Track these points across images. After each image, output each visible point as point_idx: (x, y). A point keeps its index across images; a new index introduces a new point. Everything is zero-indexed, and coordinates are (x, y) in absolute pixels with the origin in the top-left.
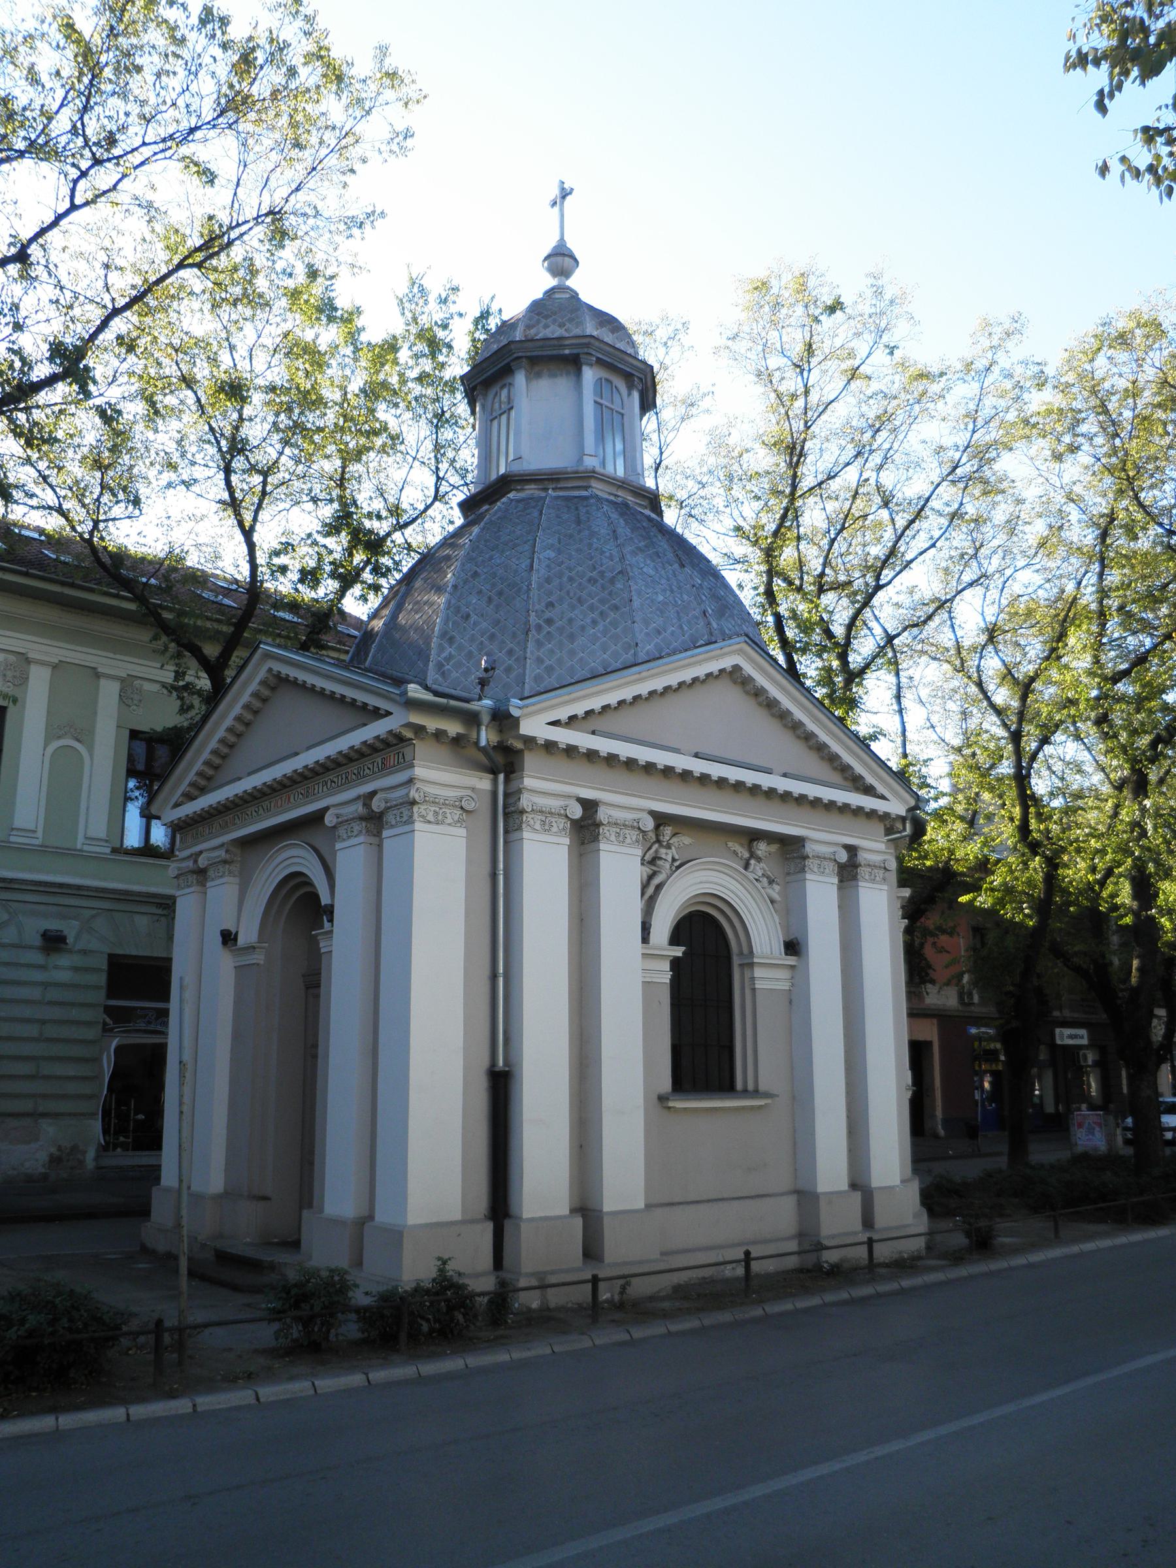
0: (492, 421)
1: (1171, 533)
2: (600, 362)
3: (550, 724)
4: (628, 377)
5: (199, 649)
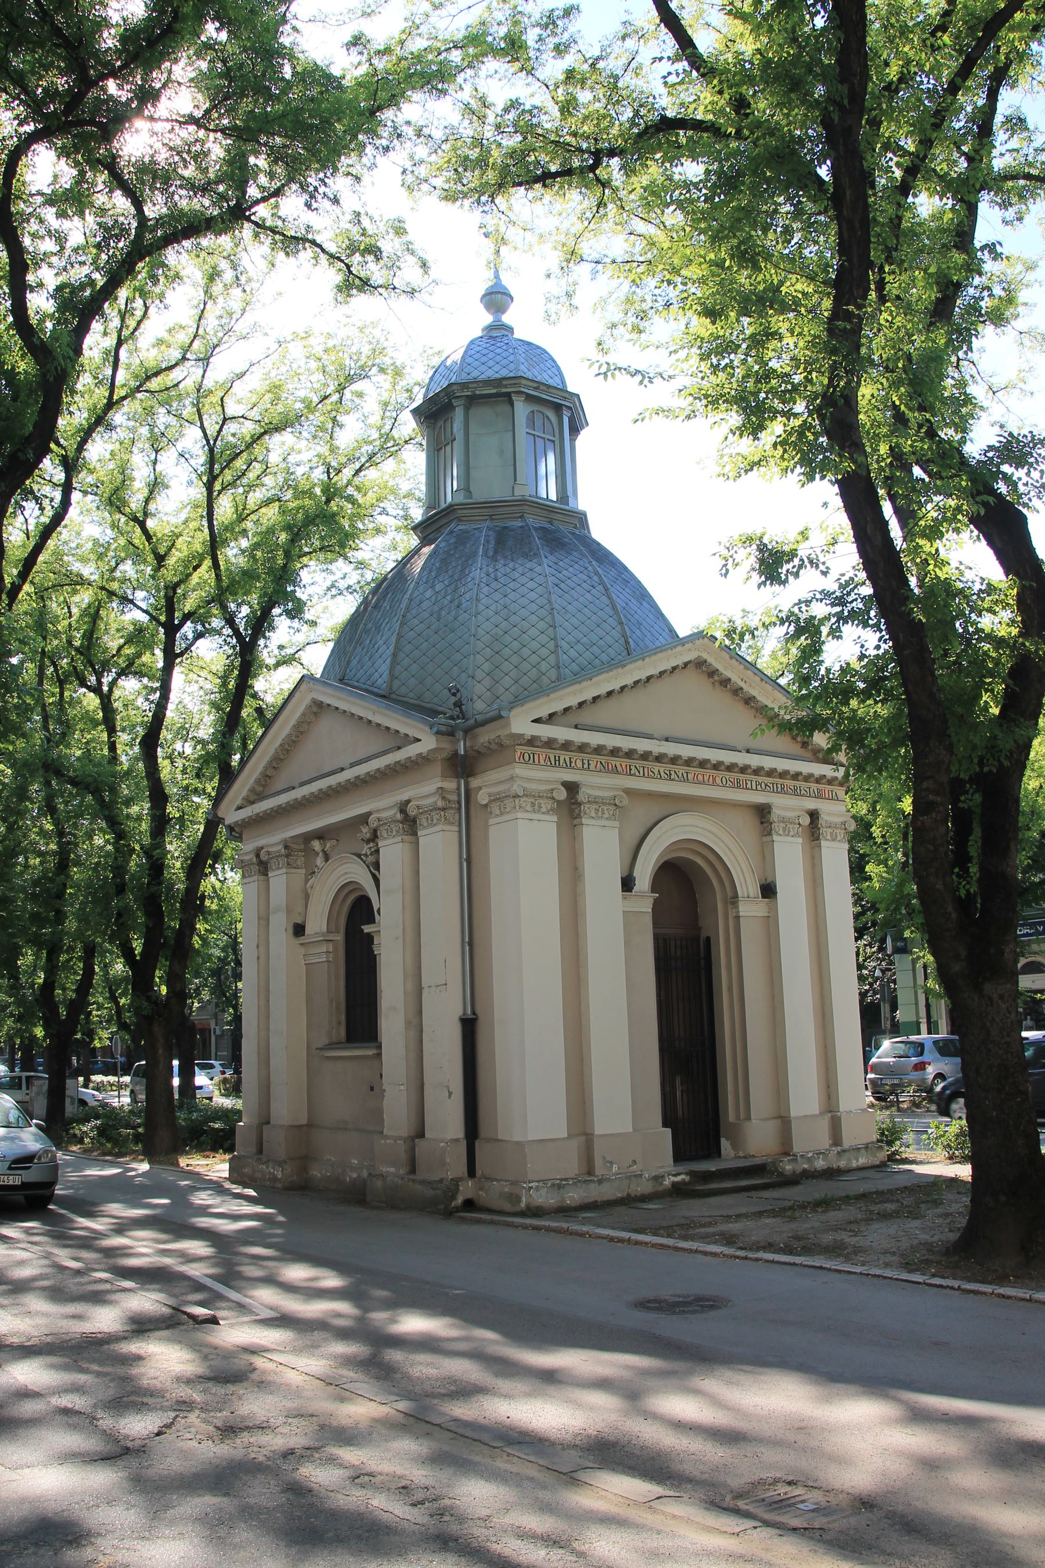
2: (530, 398)
3: (534, 721)
4: (558, 408)
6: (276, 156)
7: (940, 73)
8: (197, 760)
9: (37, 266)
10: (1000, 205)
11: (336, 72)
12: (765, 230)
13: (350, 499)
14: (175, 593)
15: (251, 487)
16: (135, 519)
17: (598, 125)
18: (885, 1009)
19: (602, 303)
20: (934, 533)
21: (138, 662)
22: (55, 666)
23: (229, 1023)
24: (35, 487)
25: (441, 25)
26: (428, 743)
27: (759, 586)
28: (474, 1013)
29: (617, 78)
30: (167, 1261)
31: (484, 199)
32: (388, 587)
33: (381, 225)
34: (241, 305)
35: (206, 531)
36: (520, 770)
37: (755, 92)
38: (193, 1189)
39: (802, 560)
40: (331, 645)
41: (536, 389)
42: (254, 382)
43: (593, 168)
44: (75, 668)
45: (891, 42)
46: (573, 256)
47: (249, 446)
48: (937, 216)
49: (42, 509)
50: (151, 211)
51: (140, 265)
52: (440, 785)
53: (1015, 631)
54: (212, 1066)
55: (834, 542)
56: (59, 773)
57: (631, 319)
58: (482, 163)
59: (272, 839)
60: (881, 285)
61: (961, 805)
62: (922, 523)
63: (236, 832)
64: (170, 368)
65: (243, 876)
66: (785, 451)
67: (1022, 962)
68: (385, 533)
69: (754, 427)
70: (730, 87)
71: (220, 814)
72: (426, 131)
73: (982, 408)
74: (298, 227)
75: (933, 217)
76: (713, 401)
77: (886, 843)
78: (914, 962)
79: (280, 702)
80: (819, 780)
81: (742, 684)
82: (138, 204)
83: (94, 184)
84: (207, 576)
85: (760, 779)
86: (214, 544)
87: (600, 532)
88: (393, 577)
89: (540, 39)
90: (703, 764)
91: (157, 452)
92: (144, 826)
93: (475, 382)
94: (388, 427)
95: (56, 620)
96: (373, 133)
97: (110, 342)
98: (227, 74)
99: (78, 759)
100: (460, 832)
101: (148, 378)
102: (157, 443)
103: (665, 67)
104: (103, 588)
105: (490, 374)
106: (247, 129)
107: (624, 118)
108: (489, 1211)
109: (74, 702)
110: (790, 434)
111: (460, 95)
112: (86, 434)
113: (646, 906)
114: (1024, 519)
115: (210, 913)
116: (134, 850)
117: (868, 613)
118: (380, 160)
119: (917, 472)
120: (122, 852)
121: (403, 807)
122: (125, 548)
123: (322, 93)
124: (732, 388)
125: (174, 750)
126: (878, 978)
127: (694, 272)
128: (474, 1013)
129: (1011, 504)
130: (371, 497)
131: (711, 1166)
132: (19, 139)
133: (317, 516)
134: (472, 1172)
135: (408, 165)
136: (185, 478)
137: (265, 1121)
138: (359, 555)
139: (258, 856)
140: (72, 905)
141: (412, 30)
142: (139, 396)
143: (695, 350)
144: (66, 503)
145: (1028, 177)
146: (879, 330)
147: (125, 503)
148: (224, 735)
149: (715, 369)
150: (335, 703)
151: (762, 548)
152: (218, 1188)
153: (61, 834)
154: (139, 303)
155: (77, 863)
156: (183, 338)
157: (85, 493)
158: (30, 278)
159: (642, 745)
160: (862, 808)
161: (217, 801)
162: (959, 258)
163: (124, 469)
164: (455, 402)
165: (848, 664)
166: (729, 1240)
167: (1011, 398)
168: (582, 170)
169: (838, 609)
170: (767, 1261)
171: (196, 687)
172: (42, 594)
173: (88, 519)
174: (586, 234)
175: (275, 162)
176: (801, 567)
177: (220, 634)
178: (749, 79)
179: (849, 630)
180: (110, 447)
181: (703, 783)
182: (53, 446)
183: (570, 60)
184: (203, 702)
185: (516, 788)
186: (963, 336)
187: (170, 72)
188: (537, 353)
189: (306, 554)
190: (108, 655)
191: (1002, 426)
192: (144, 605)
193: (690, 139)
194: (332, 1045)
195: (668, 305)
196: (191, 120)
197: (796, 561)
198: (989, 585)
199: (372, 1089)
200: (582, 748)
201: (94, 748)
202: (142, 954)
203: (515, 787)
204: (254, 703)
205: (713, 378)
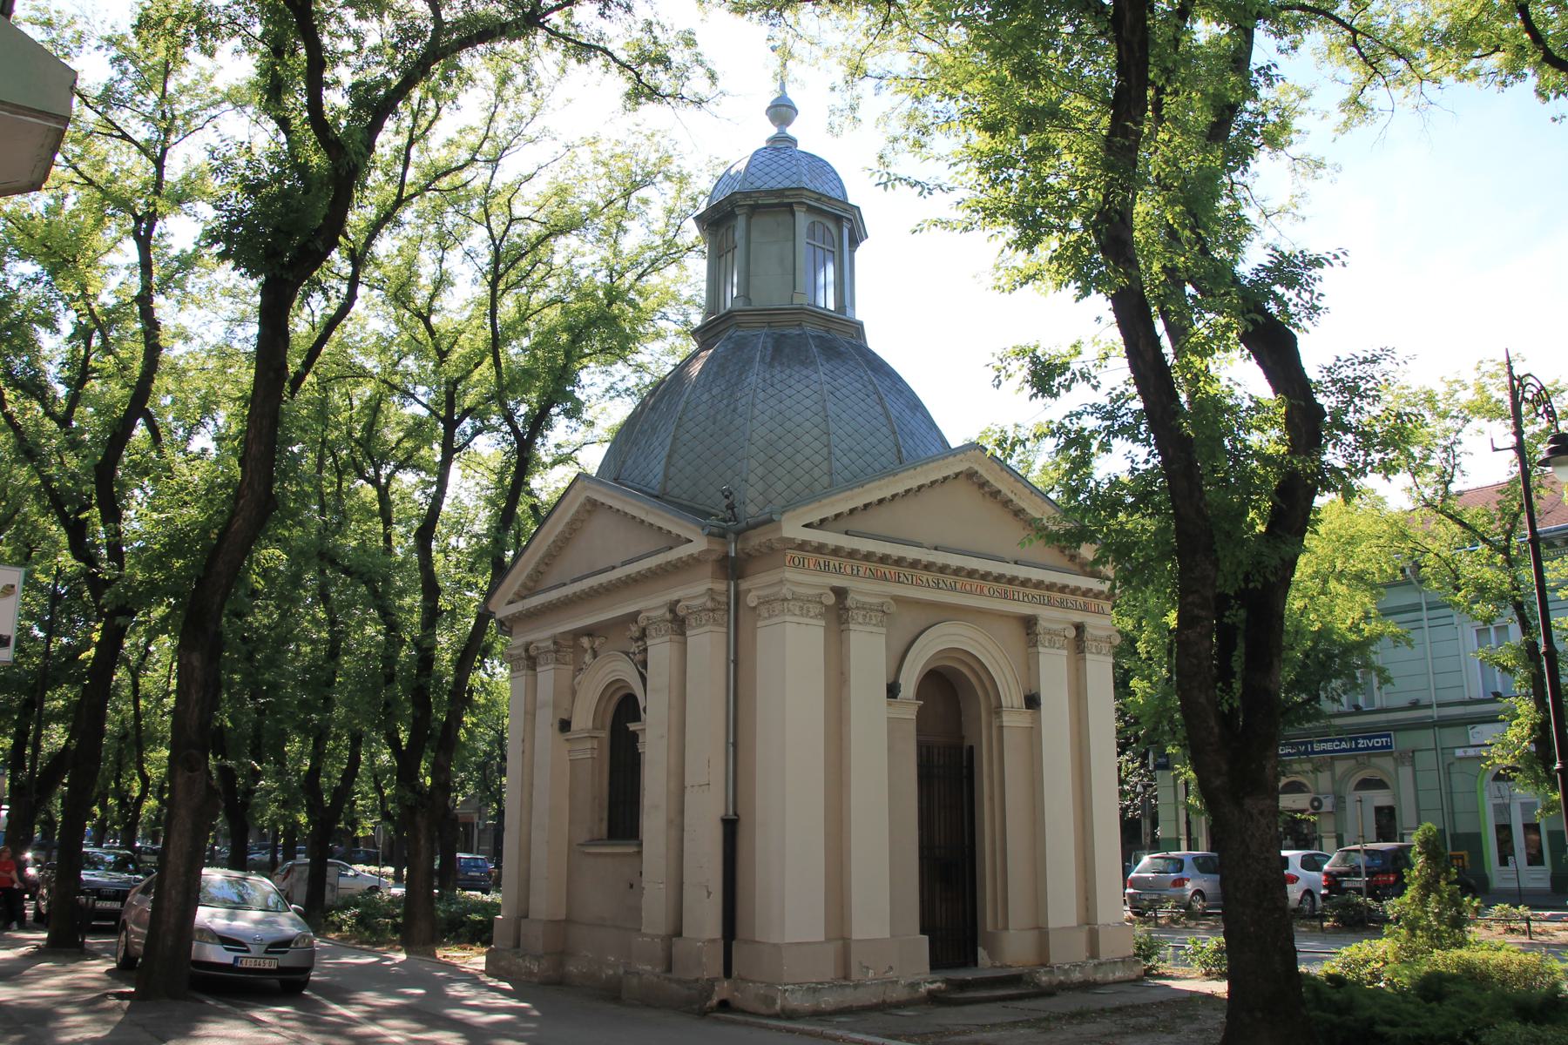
0: (720, 257)
2: (811, 209)
3: (805, 526)
4: (838, 220)
9: (335, 64)
10: (1275, 34)
13: (632, 303)
14: (456, 388)
15: (535, 288)
16: (420, 315)
18: (1146, 825)
20: (1204, 350)
23: (492, 818)
26: (699, 544)
27: (1031, 398)
28: (735, 814)
31: (772, 12)
32: (665, 390)
35: (489, 329)
36: (790, 574)
38: (450, 980)
39: (1074, 374)
40: (607, 445)
41: (818, 200)
44: (354, 459)
47: (534, 247)
48: (1215, 42)
52: (710, 585)
53: (1283, 449)
55: (1106, 357)
56: (333, 562)
57: (913, 134)
59: (542, 635)
61: (1225, 620)
63: (506, 627)
67: (1283, 781)
69: (1028, 243)
76: (991, 214)
77: (1151, 659)
78: (1176, 777)
80: (1087, 593)
81: (1012, 496)
85: (1027, 590)
87: (876, 342)
88: (671, 381)
90: (971, 574)
91: (444, 249)
92: (416, 618)
94: (671, 234)
97: (402, 140)
99: (354, 549)
100: (728, 634)
101: (437, 177)
102: (445, 241)
104: (385, 381)
108: (744, 1012)
110: (1066, 249)
112: (375, 229)
113: (908, 711)
114: (1294, 338)
115: (478, 707)
117: (1138, 429)
119: (1189, 289)
122: (408, 343)
126: (1139, 794)
127: (974, 87)
128: (735, 814)
129: (1281, 324)
130: (652, 302)
131: (967, 975)
134: (728, 972)
139: (527, 650)
142: (428, 194)
143: (975, 164)
144: (352, 297)
147: (410, 299)
148: (498, 529)
149: (994, 183)
150: (609, 502)
151: (1035, 360)
152: (473, 980)
154: (431, 104)
155: (348, 652)
156: (473, 139)
158: (328, 75)
159: (911, 553)
160: (1128, 624)
161: (488, 595)
163: (411, 264)
167: (1284, 223)
169: (1109, 423)
172: (325, 385)
173: (373, 313)
176: (1072, 380)
179: (1120, 445)
180: (398, 243)
181: (971, 592)
182: (341, 239)
184: (479, 498)
186: (1241, 155)
189: (586, 355)
194: (593, 842)
197: (1068, 375)
198: (1257, 402)
199: (631, 886)
200: (852, 554)
203: (784, 591)
204: (530, 501)
205: (991, 191)
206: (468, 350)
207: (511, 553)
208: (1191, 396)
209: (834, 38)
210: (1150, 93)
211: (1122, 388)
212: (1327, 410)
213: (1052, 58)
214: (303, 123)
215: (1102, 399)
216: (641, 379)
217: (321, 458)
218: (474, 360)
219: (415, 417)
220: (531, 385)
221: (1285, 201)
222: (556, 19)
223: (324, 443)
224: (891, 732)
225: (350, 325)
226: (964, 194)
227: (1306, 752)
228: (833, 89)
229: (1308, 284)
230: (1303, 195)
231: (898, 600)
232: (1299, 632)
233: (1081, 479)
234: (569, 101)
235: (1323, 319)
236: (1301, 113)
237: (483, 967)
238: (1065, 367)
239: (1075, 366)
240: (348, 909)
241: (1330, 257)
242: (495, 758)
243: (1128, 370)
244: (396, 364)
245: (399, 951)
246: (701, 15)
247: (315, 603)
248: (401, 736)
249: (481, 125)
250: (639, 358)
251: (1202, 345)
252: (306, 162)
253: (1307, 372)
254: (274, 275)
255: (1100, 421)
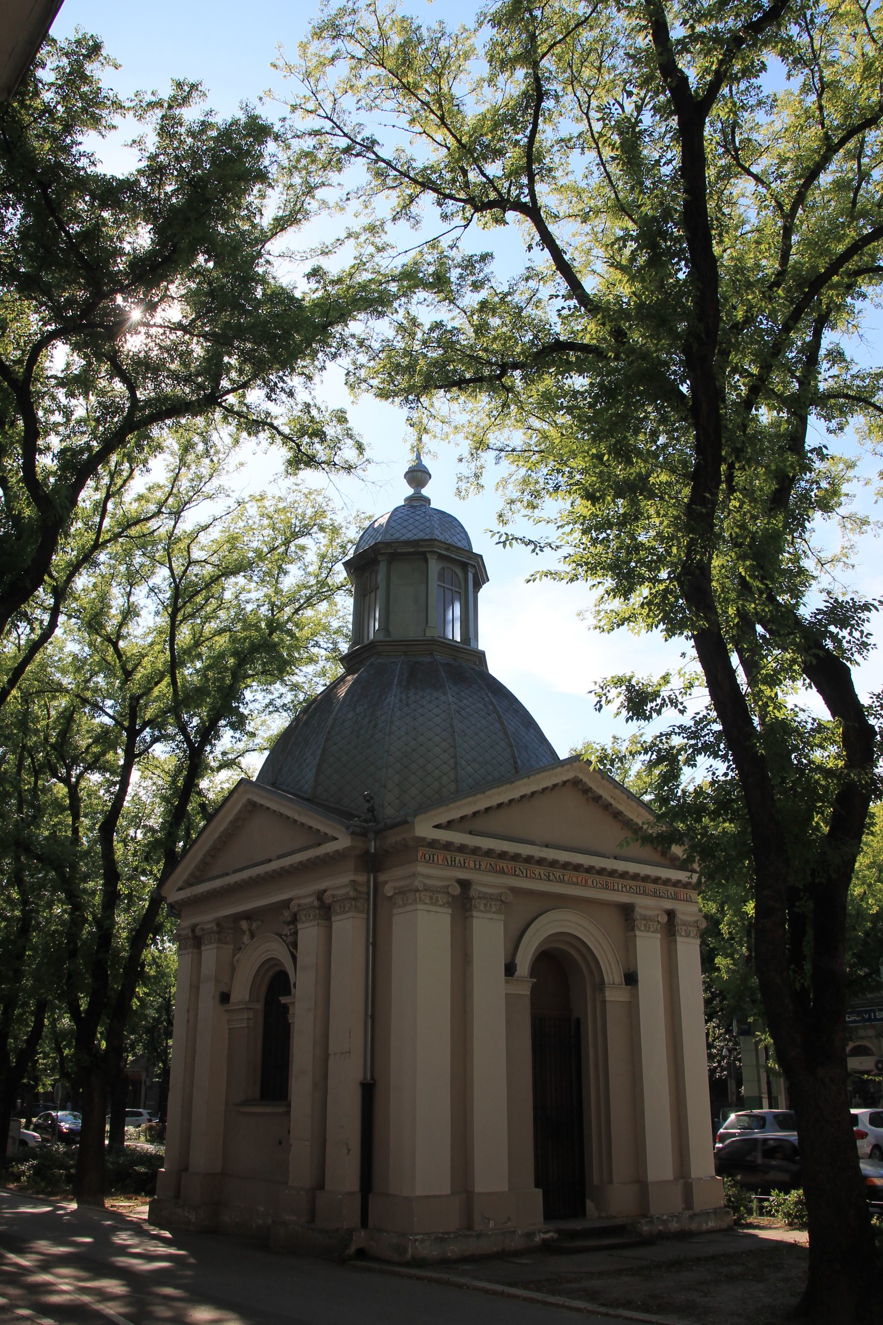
0: (365, 596)
1: (880, 901)
2: (441, 557)
4: (464, 566)
5: (123, 766)
6: (246, 357)
7: (776, 316)
8: (146, 845)
9: (46, 434)
10: (825, 418)
11: (298, 294)
12: (636, 432)
13: (290, 633)
14: (138, 703)
15: (207, 619)
16: (109, 640)
17: (505, 344)
18: (732, 1084)
19: (503, 483)
20: (773, 681)
21: (102, 759)
22: (33, 759)
23: (158, 1076)
24: (29, 610)
25: (384, 263)
26: (343, 842)
27: (627, 721)
28: (373, 1078)
29: (521, 309)
30: (86, 1299)
31: (411, 397)
32: (316, 708)
33: (327, 414)
34: (209, 471)
35: (168, 653)
36: (421, 868)
37: (631, 326)
38: (114, 1230)
39: (663, 699)
40: (267, 753)
41: (447, 549)
42: (215, 533)
43: (499, 377)
44: (49, 761)
45: (738, 292)
46: (481, 445)
47: (208, 586)
48: (776, 424)
49: (32, 630)
50: (141, 395)
51: (130, 436)
52: (352, 877)
53: (841, 764)
54: (140, 1114)
55: (691, 686)
56: (28, 850)
57: (527, 497)
58: (410, 369)
59: (207, 918)
60: (730, 478)
61: (796, 909)
62: (764, 672)
63: (175, 910)
64: (148, 519)
65: (180, 949)
66: (650, 610)
67: (851, 1045)
68: (317, 662)
69: (624, 590)
70: (611, 321)
71: (164, 894)
72: (367, 343)
73: (814, 578)
74: (259, 412)
75: (772, 425)
76: (593, 568)
77: (733, 939)
78: (757, 1043)
79: (220, 799)
80: (677, 884)
81: (611, 801)
82: (132, 388)
83: (98, 371)
84: (166, 691)
85: (626, 882)
86: (175, 664)
87: (496, 669)
88: (322, 700)
89: (461, 276)
90: (577, 868)
91: (131, 585)
92: (97, 900)
93: (398, 542)
94: (324, 575)
95: (36, 719)
96: (325, 343)
97: (99, 496)
98: (211, 293)
99: (46, 838)
100: (368, 919)
101: (129, 526)
102: (133, 579)
103: (559, 303)
104: (78, 696)
105: (410, 536)
106: (224, 335)
107: (526, 340)
108: (378, 1260)
109: (46, 790)
110: (655, 596)
111: (395, 317)
112: (74, 569)
113: (524, 990)
114: (848, 670)
115: (149, 978)
116: (87, 920)
117: (718, 746)
118: (328, 364)
119: (759, 629)
120: (77, 922)
121: (320, 895)
122: (99, 664)
123: (285, 310)
124: (608, 557)
125: (128, 835)
126: (725, 1057)
127: (578, 463)
128: (373, 1078)
129: (837, 658)
130: (306, 632)
131: (576, 1225)
132: (42, 335)
133: (261, 646)
134: (365, 1222)
135: (351, 368)
136: (153, 608)
137: (183, 1167)
138: (297, 679)
139: (193, 931)
140: (29, 965)
141: (360, 265)
142: (120, 540)
143: (578, 526)
144: (53, 624)
145: (846, 396)
146: (729, 514)
147: (102, 626)
148: (171, 825)
149: (594, 542)
150: (267, 804)
151: (630, 688)
152: (137, 1228)
153: (25, 902)
154: (126, 466)
155: (37, 928)
156: (159, 495)
157: (70, 617)
158: (40, 442)
159: (525, 850)
160: (712, 907)
161: (161, 882)
162: (792, 458)
163: (104, 599)
164: (380, 558)
165: (701, 788)
166: (592, 1296)
167: (837, 570)
168: (491, 379)
169: (692, 742)
170: (626, 1318)
171: (150, 782)
172: (27, 698)
173: (70, 638)
174: (493, 428)
175: (244, 362)
176: (662, 705)
177: (173, 740)
178: (624, 314)
179: (703, 760)
180: (93, 580)
181: (576, 884)
182: (46, 578)
183: (483, 294)
184: (155, 796)
185: (417, 883)
186: (798, 522)
187: (167, 289)
188: (449, 522)
189: (250, 676)
190: (77, 752)
191: (829, 593)
192: (110, 711)
193: (577, 358)
194: (247, 1102)
195: (557, 488)
196: (179, 326)
197: (659, 701)
198: (819, 724)
199: (280, 1143)
200: (475, 851)
201: (60, 830)
202: (86, 1011)
203: (416, 883)
204: (199, 800)
205: (592, 549)
206: (149, 671)
207: (181, 844)
208: (762, 723)
209: (461, 418)
210: (723, 467)
211: (705, 713)
212: (877, 729)
213: (641, 441)
214: (18, 482)
215: (687, 720)
216: (296, 696)
217: (21, 760)
218: (154, 680)
219: (102, 725)
220: (202, 701)
221: (837, 551)
222: (231, 399)
223: (24, 747)
224: (508, 1004)
225: (50, 647)
226: (567, 550)
227: (870, 1019)
228: (461, 460)
229: (858, 624)
230: (852, 547)
231: (514, 890)
232: (861, 914)
233: (671, 790)
234: (242, 464)
235: (872, 654)
236: (848, 481)
237: (146, 1217)
238: (656, 694)
239: (665, 693)
240: (27, 1161)
241: (876, 603)
242: (162, 1023)
243: (709, 698)
244: (88, 681)
245: (71, 1200)
246: (352, 398)
247: (10, 884)
248: (81, 1002)
249: (166, 483)
250: (295, 679)
251: (771, 676)
252: (20, 513)
253: (859, 697)
254: (69, 1179)
255: (686, 741)
